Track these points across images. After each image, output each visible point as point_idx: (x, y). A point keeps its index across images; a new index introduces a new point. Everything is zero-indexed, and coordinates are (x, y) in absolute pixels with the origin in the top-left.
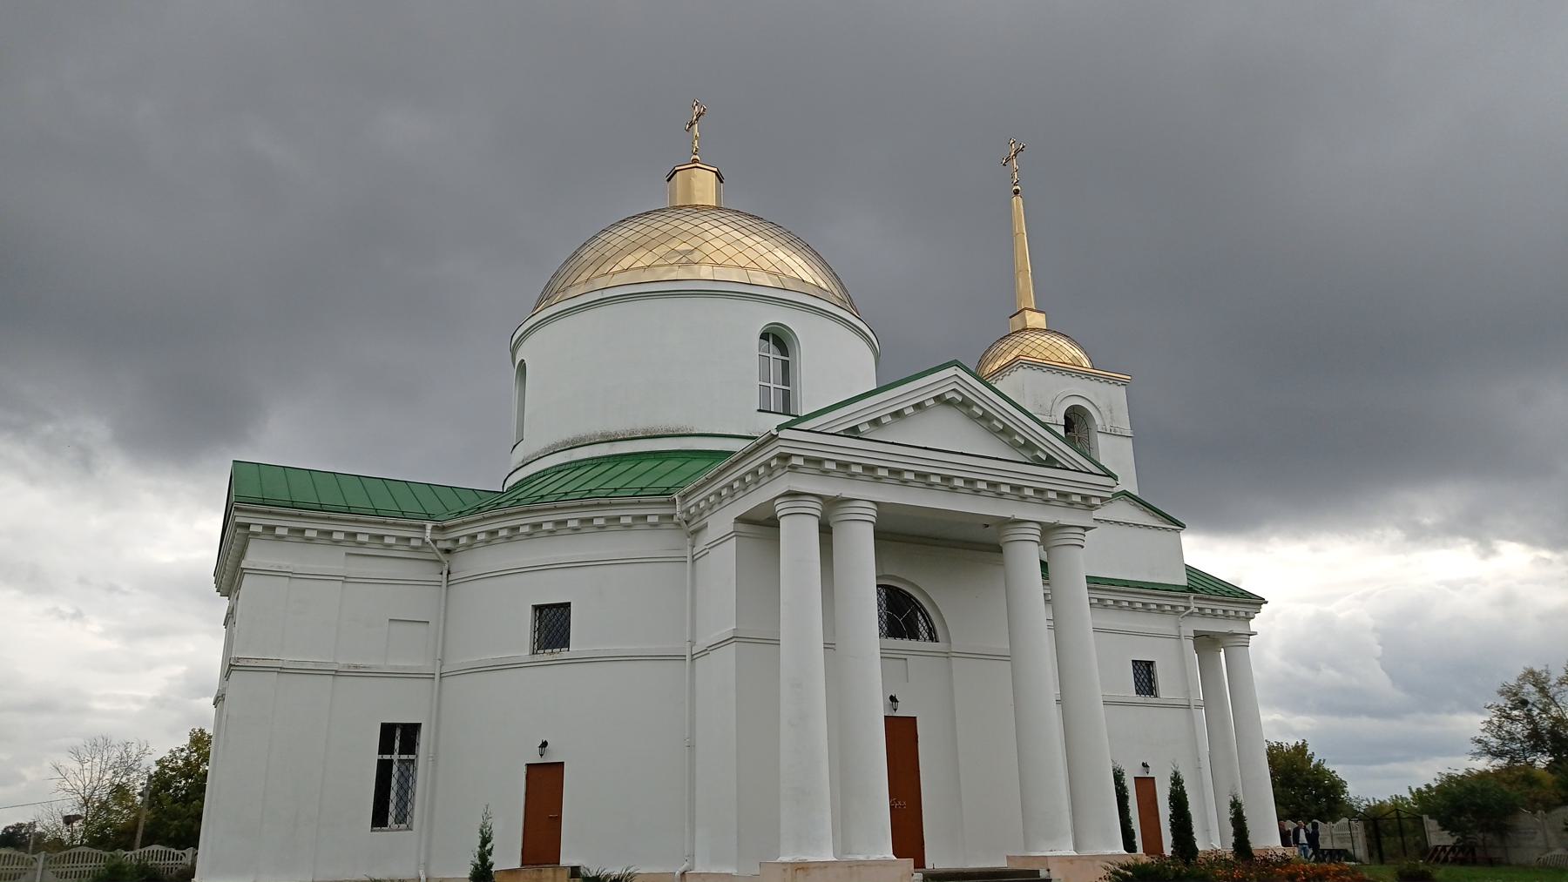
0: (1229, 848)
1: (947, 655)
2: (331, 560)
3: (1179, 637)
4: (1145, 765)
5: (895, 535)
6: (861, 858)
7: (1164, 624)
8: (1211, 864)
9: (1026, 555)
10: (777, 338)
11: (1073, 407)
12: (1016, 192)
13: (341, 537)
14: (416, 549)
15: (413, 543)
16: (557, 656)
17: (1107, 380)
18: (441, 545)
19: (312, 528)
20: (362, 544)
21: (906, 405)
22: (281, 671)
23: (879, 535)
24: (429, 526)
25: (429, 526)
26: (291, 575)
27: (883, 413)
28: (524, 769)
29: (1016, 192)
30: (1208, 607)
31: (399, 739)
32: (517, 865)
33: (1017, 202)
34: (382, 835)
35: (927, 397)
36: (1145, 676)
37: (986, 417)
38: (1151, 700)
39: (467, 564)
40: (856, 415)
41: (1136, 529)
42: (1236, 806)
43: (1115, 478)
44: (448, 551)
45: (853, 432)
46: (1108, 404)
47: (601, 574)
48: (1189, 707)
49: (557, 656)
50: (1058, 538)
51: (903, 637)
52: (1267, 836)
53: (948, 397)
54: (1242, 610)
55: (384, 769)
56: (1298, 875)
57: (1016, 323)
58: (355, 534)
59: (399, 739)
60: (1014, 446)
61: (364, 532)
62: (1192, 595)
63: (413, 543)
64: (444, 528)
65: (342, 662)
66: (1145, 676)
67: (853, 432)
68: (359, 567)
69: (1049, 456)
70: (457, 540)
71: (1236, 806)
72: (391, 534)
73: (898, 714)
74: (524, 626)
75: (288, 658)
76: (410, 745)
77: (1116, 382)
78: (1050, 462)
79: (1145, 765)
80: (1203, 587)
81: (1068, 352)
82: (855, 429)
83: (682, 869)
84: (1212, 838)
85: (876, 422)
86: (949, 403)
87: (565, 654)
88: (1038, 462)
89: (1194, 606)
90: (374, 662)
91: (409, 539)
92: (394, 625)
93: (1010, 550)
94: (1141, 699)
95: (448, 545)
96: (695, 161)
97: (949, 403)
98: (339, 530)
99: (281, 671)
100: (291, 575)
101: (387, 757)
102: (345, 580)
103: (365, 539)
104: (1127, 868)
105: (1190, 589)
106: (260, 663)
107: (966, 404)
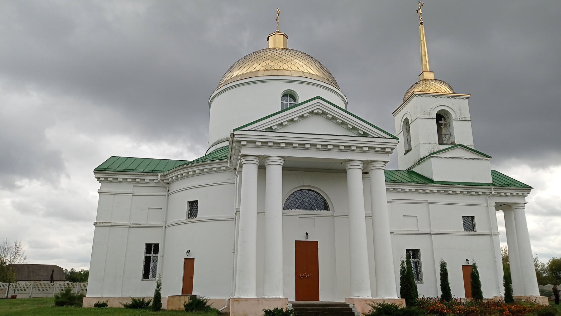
1: (333, 216)
3: (487, 206)
4: (467, 260)
5: (291, 169)
6: (266, 297)
7: (481, 200)
9: (355, 176)
11: (442, 110)
12: (421, 23)
13: (130, 180)
14: (156, 183)
15: (155, 181)
16: (193, 220)
17: (458, 97)
18: (165, 181)
19: (120, 178)
20: (138, 182)
21: (295, 117)
22: (111, 226)
23: (285, 169)
24: (159, 175)
25: (159, 175)
26: (115, 194)
27: (284, 120)
28: (183, 260)
29: (421, 23)
30: (502, 192)
31: (152, 249)
32: (181, 294)
33: (422, 27)
34: (146, 282)
35: (305, 112)
36: (469, 223)
37: (333, 118)
38: (473, 233)
40: (272, 122)
41: (451, 159)
43: (398, 139)
44: (168, 183)
45: (270, 129)
46: (458, 108)
47: (208, 191)
48: (491, 235)
49: (193, 220)
50: (372, 166)
51: (314, 209)
52: (459, 292)
53: (315, 111)
54: (525, 192)
55: (147, 261)
56: (504, 310)
57: (421, 78)
58: (135, 179)
59: (152, 249)
60: (348, 129)
61: (138, 178)
62: (493, 188)
63: (155, 181)
64: (165, 175)
65: (132, 223)
66: (469, 223)
67: (270, 129)
69: (364, 132)
70: (168, 179)
72: (147, 178)
73: (309, 240)
74: (185, 208)
75: (113, 222)
76: (156, 252)
77: (463, 98)
78: (365, 135)
79: (467, 260)
80: (502, 183)
81: (445, 89)
82: (271, 128)
83: (229, 298)
84: (493, 290)
85: (281, 124)
86: (317, 114)
87: (195, 219)
88: (360, 136)
89: (493, 192)
90: (143, 223)
91: (154, 180)
92: (150, 210)
93: (348, 172)
94: (466, 232)
95: (167, 181)
96: (277, 32)
97: (317, 114)
98: (130, 178)
99: (111, 226)
100: (115, 194)
101: (148, 255)
102: (133, 195)
103: (138, 180)
104: (380, 305)
105: (493, 185)
106: (104, 224)
107: (324, 113)
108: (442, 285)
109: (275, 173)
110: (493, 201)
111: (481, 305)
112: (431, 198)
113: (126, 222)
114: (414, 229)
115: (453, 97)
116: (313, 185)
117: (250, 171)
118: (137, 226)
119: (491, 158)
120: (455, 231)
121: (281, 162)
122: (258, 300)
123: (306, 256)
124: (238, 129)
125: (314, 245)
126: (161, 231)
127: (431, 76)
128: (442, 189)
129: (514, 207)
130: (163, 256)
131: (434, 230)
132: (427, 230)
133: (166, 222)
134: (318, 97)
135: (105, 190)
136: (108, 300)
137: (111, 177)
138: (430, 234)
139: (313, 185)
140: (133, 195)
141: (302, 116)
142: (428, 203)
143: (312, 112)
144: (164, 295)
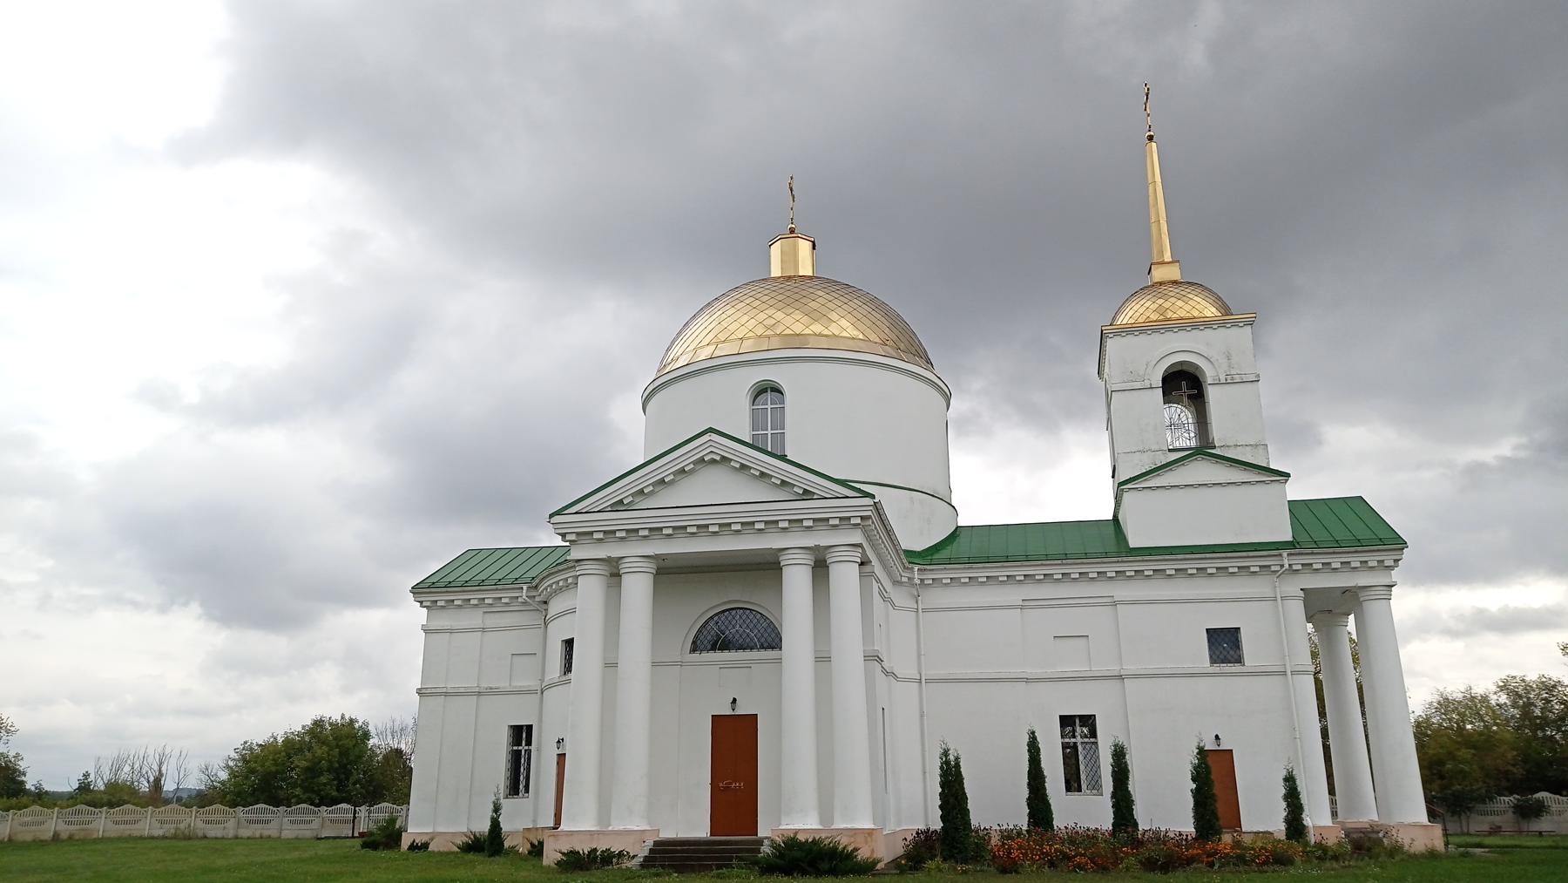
0: (1023, 823)
2: (473, 618)
5: (668, 573)
8: (1179, 845)
9: (797, 579)
10: (767, 390)
11: (1181, 363)
12: (1151, 138)
19: (458, 599)
22: (446, 694)
26: (451, 631)
30: (1317, 562)
31: (521, 734)
36: (1225, 644)
38: (1236, 668)
39: (555, 607)
42: (1290, 780)
45: (618, 506)
48: (1284, 673)
59: (521, 734)
61: (489, 597)
66: (1225, 644)
67: (618, 506)
68: (493, 621)
71: (1290, 780)
72: (506, 596)
73: (739, 712)
75: (451, 685)
78: (807, 495)
84: (1261, 814)
90: (503, 684)
94: (1216, 668)
97: (713, 461)
99: (446, 694)
100: (451, 631)
102: (483, 630)
108: (1114, 795)
109: (638, 588)
110: (1294, 587)
111: (1138, 843)
112: (1121, 591)
113: (472, 684)
114: (1080, 668)
115: (1223, 324)
116: (727, 605)
117: (590, 588)
118: (493, 692)
119: (1288, 475)
120: (1187, 666)
121: (651, 567)
122: (598, 833)
123: (735, 743)
124: (558, 513)
125: (749, 723)
126: (536, 698)
127: (1174, 273)
128: (1148, 568)
129: (1363, 595)
130: (539, 744)
131: (1130, 668)
132: (1114, 669)
133: (542, 680)
134: (711, 430)
135: (436, 624)
136: (433, 836)
137: (442, 599)
138: (1120, 677)
139: (727, 605)
140: (483, 630)
141: (682, 471)
142: (1115, 604)
143: (702, 460)
144: (505, 826)
